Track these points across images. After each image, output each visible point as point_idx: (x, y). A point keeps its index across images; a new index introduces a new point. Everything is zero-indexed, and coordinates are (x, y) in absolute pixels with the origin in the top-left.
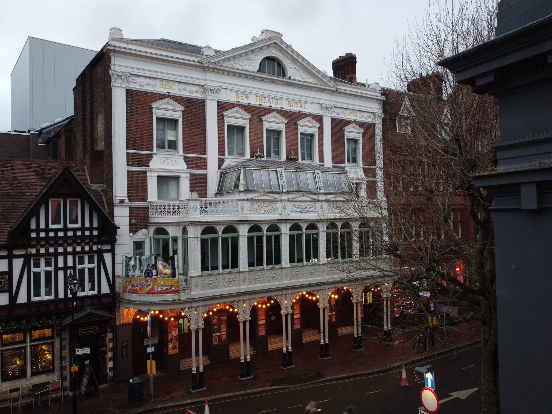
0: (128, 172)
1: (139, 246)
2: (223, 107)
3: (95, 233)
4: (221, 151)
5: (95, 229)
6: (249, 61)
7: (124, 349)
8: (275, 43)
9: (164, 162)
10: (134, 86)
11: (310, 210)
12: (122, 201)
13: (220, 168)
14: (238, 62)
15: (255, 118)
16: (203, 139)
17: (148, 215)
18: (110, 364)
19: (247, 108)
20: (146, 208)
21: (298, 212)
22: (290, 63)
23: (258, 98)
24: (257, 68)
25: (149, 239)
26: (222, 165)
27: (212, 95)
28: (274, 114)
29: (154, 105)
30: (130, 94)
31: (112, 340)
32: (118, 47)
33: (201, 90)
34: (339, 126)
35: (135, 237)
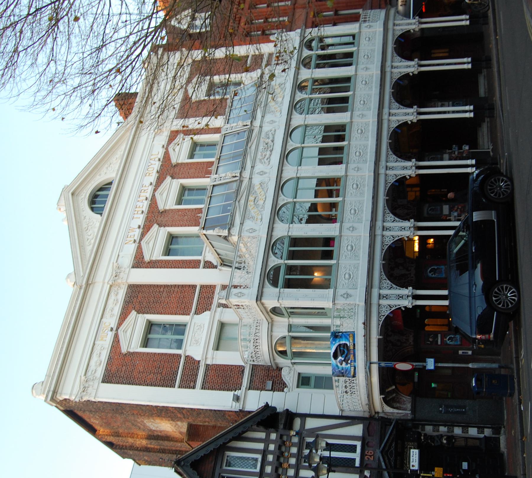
0: (203, 388)
1: (304, 381)
2: (139, 262)
3: (273, 436)
4: (195, 264)
5: (268, 436)
6: (89, 227)
7: (450, 410)
8: (73, 194)
9: (198, 341)
10: (100, 372)
11: (271, 139)
12: (237, 399)
13: (216, 267)
14: (89, 240)
15: (159, 219)
16: (176, 289)
17: (263, 366)
18: (473, 432)
19: (146, 229)
20: (254, 368)
21: (270, 155)
22: (100, 175)
23: (136, 216)
24: (99, 216)
25: (295, 366)
26: (212, 264)
27: (122, 275)
28: (157, 194)
29: (124, 350)
30: (109, 378)
31: (436, 426)
32: (50, 387)
33: (116, 289)
34: (188, 108)
35: (291, 385)
